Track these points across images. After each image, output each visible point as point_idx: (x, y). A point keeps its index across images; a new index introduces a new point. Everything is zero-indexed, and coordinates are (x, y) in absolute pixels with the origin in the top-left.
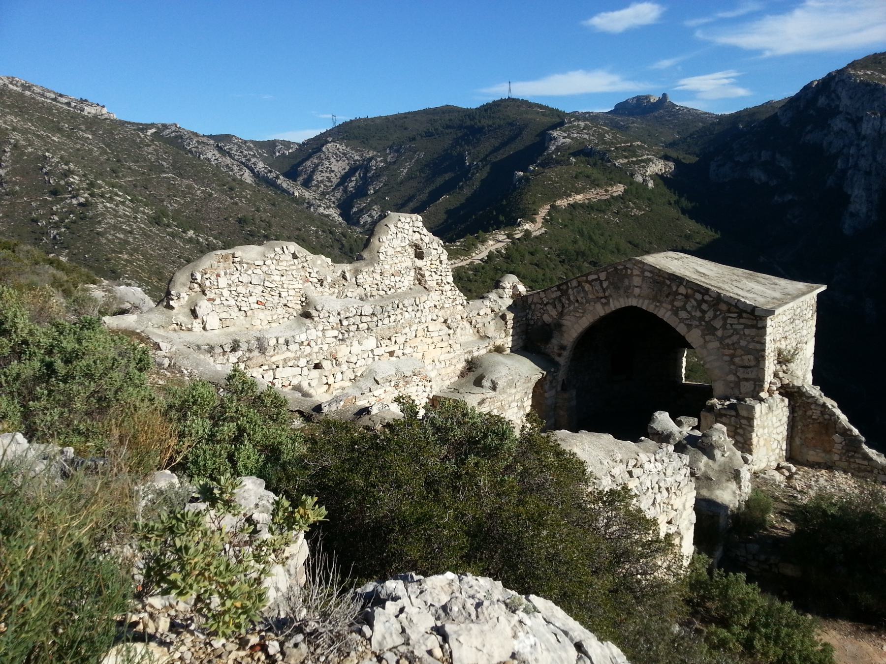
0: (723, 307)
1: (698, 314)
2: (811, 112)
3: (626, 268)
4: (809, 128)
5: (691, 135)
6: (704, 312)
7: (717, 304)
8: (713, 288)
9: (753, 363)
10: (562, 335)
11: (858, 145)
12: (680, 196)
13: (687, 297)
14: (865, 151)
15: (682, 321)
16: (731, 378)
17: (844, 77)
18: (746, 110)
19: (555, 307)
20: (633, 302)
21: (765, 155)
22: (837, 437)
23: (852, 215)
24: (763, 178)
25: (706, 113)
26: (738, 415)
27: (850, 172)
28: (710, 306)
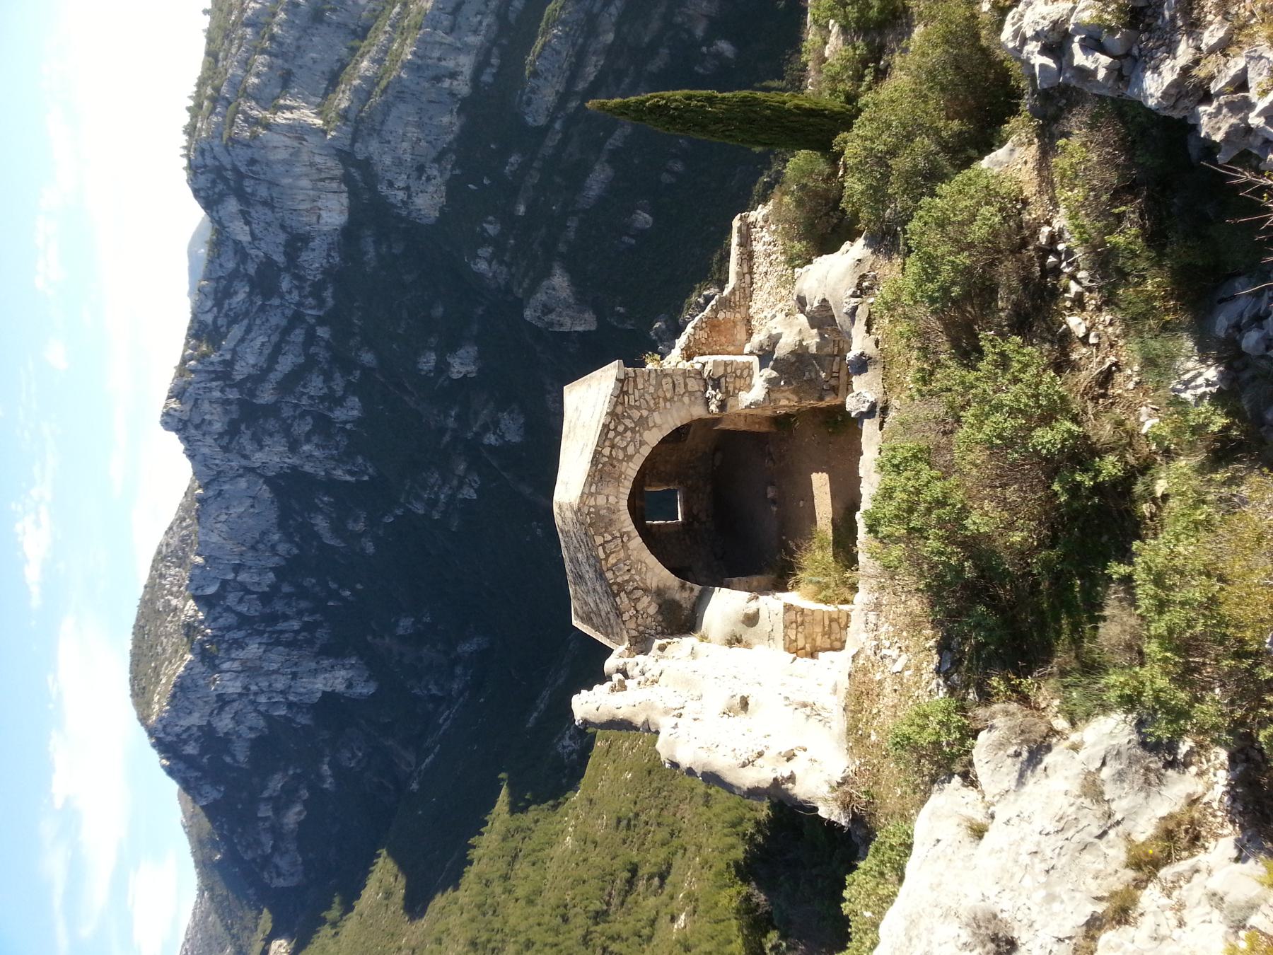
0: (619, 409)
1: (629, 434)
2: (205, 760)
3: (589, 513)
4: (228, 759)
5: (228, 928)
6: (626, 429)
7: (617, 415)
8: (602, 421)
9: (669, 380)
10: (669, 588)
11: (256, 694)
12: (323, 921)
13: (613, 446)
14: (264, 684)
15: (637, 451)
16: (686, 399)
17: (160, 727)
18: (194, 854)
19: (638, 599)
20: (624, 504)
21: (265, 811)
22: (721, 315)
23: (350, 685)
24: (298, 808)
25: (194, 914)
26: (724, 376)
27: (291, 698)
28: (620, 423)
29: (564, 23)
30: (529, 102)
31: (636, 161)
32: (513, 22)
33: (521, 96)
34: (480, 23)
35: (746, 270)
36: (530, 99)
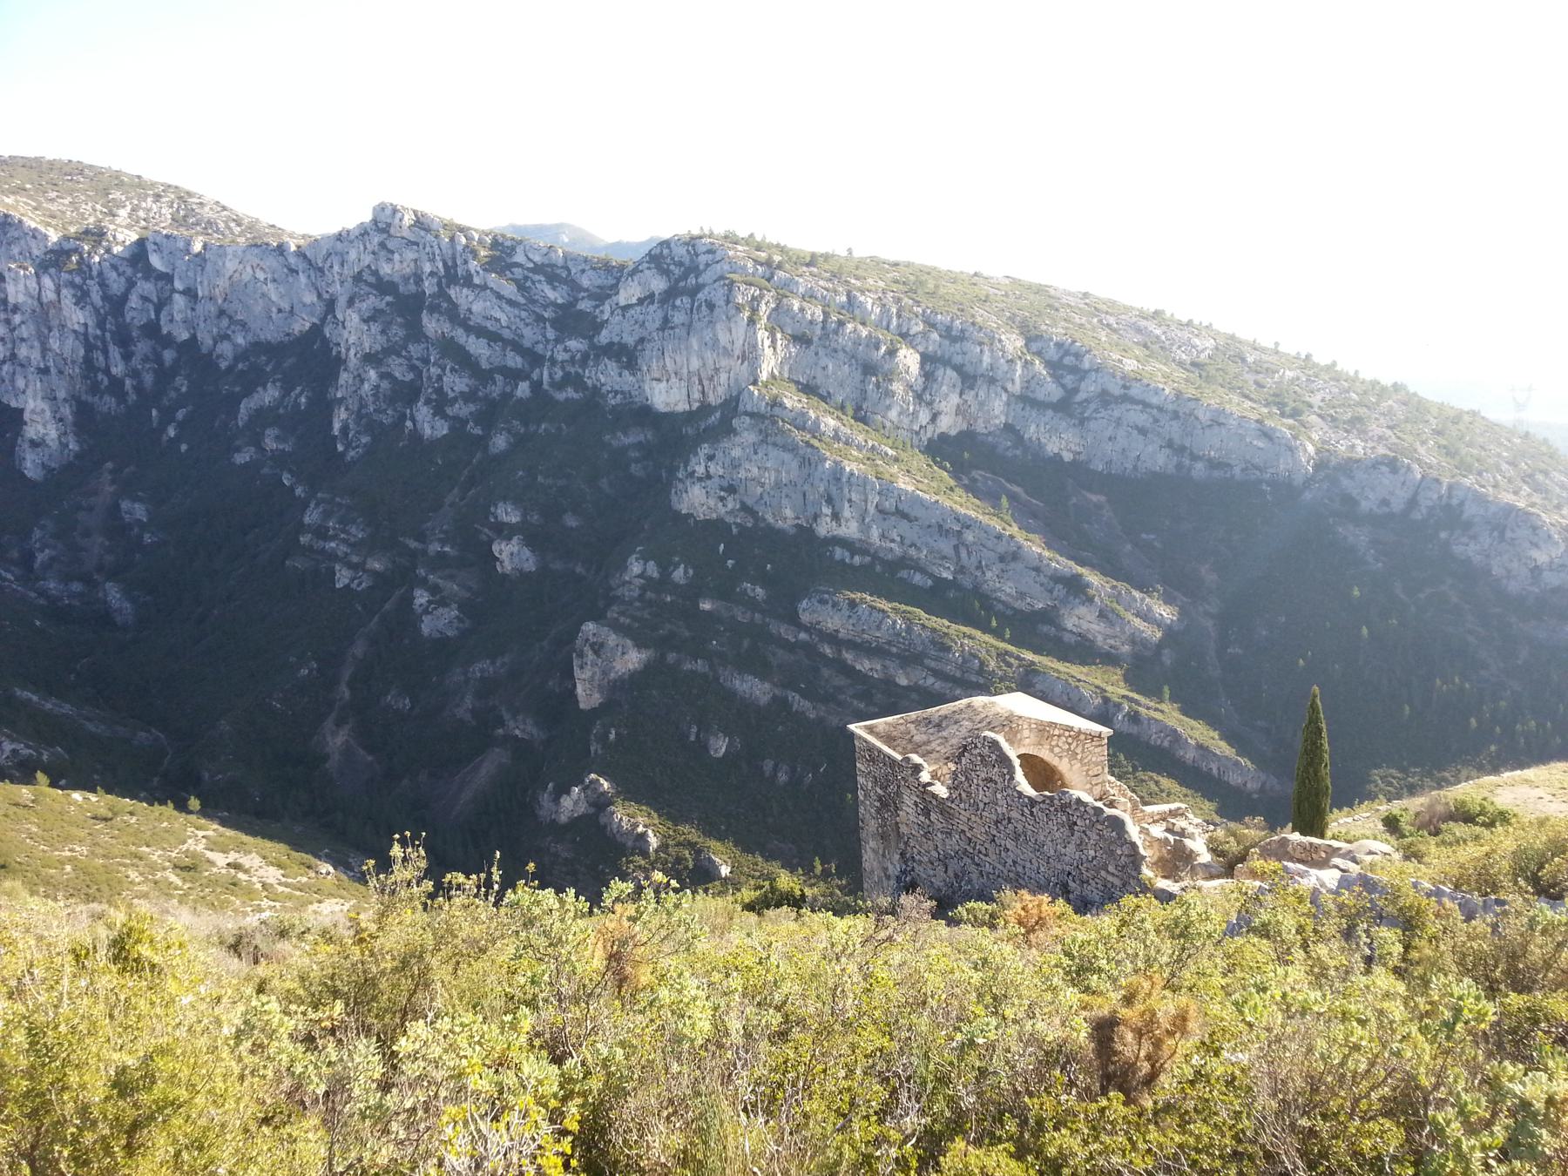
29: (909, 630)
30: (822, 602)
34: (893, 541)
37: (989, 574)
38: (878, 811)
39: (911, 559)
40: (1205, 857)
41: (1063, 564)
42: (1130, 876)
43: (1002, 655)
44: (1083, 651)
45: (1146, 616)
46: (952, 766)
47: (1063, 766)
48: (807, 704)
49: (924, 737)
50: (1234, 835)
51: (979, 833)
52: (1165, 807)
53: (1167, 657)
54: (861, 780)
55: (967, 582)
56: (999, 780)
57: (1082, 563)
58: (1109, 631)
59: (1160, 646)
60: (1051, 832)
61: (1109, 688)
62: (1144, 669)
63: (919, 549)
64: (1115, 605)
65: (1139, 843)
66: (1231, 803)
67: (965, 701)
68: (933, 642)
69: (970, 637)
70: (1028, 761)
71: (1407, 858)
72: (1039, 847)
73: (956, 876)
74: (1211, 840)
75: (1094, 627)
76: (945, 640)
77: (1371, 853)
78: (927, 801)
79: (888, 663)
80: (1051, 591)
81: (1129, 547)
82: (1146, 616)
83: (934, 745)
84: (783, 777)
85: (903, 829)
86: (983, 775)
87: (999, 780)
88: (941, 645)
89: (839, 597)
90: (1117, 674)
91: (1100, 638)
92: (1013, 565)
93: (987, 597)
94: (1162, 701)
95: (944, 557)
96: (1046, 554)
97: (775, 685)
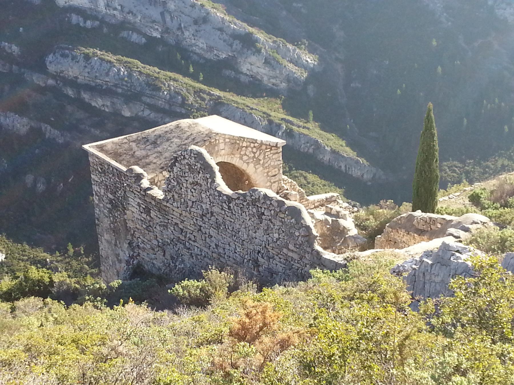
0: (264, 147)
3: (216, 140)
13: (246, 147)
29: (130, 75)
30: (64, 56)
31: (37, 151)
32: (121, 35)
33: (68, 49)
34: (115, 9)
35: (316, 205)
36: (67, 56)
37: (187, 34)
38: (110, 211)
39: (130, 23)
40: (354, 231)
41: (238, 26)
42: (306, 252)
43: (198, 92)
44: (254, 88)
45: (296, 62)
46: (166, 174)
47: (250, 169)
48: (57, 132)
49: (144, 153)
50: (372, 214)
51: (189, 225)
52: (323, 196)
53: (311, 89)
54: (95, 188)
55: (171, 40)
56: (203, 183)
57: (252, 25)
58: (272, 73)
59: (307, 82)
60: (244, 221)
61: (273, 114)
62: (297, 100)
63: (135, 15)
64: (276, 55)
65: (312, 226)
66: (359, 193)
67: (174, 123)
68: (148, 84)
69: (175, 80)
70: (224, 167)
71: (502, 228)
72: (235, 233)
73: (172, 258)
74: (356, 218)
75: (262, 71)
76: (157, 82)
77: (474, 223)
78: (149, 204)
79: (115, 100)
80: (231, 45)
81: (284, 13)
82: (296, 62)
83: (151, 158)
84: (41, 187)
85: (130, 224)
86: (191, 180)
87: (203, 183)
88: (153, 86)
89: (77, 52)
90: (277, 104)
91: (265, 78)
92: (203, 26)
93: (186, 50)
94: (308, 122)
95: (154, 22)
96: (227, 18)
97: (31, 119)
